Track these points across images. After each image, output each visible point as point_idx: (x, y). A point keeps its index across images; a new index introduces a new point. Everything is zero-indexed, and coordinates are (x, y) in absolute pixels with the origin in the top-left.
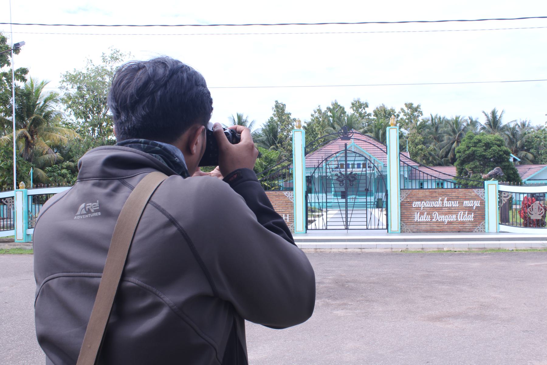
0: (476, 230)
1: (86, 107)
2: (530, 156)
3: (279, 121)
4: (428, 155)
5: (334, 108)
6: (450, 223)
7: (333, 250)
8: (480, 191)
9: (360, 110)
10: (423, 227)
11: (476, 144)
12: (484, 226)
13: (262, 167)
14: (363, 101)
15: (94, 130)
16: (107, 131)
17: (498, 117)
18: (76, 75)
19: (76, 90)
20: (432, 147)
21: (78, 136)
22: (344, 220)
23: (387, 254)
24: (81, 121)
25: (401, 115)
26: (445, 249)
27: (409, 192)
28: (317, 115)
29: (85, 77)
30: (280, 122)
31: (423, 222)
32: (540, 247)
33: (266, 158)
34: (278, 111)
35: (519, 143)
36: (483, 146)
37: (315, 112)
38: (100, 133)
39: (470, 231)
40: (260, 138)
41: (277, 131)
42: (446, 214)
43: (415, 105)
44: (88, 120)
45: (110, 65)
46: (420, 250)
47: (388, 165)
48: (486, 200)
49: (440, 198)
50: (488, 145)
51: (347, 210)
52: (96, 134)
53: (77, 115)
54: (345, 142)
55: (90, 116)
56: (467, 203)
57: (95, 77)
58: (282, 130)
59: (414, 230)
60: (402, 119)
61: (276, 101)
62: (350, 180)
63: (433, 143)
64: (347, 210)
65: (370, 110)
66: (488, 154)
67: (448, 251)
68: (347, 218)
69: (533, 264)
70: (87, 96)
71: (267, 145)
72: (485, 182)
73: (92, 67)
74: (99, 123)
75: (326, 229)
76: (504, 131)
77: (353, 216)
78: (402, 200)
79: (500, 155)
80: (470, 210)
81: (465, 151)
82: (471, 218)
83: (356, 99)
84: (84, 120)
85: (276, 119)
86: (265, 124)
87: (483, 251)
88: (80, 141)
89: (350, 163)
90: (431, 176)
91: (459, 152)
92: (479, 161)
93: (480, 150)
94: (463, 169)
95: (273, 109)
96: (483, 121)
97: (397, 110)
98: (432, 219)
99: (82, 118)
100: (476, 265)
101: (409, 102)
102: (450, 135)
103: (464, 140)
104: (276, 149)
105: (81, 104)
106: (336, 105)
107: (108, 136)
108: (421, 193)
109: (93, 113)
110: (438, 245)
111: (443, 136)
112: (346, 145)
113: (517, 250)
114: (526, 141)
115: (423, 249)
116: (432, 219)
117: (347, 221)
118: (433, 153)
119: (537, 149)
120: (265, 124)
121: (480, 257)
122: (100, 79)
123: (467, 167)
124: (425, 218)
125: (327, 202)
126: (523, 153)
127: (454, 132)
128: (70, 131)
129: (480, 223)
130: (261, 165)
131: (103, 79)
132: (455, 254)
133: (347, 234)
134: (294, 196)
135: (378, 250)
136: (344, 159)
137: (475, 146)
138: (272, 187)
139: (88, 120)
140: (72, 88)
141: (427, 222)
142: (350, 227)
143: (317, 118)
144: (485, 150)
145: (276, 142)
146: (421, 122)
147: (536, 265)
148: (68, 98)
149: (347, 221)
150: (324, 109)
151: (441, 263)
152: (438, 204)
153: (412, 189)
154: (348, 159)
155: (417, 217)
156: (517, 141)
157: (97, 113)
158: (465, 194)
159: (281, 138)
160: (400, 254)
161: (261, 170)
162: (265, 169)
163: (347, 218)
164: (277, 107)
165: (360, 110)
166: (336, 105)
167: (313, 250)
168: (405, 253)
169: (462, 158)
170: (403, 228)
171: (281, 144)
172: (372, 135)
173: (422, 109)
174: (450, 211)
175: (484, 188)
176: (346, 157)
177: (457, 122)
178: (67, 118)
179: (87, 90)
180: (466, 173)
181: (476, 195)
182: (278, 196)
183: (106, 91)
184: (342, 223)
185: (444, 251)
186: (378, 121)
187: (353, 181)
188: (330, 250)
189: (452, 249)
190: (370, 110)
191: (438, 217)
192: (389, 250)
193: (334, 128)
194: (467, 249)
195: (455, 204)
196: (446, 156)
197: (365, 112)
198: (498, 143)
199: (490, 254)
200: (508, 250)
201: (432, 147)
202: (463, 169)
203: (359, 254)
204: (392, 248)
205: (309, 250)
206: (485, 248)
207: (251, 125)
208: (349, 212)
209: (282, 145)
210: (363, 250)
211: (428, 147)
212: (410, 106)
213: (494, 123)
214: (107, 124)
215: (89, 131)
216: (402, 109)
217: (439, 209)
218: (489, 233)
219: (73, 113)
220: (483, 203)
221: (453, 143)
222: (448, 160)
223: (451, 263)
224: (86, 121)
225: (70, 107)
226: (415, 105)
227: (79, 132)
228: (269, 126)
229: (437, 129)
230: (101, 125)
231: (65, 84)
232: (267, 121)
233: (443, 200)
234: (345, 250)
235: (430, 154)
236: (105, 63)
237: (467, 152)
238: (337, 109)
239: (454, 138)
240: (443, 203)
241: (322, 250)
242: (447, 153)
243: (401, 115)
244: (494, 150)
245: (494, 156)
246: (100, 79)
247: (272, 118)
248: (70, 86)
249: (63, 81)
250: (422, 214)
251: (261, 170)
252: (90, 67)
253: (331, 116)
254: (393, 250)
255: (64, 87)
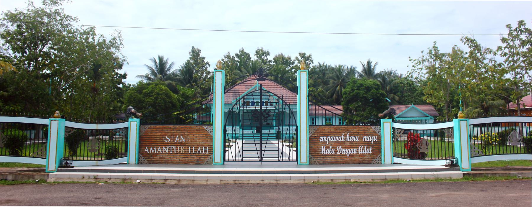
0: (373, 162)
1: (24, 43)
2: (397, 98)
3: (194, 64)
4: (317, 96)
5: (241, 55)
6: (352, 155)
7: (251, 182)
8: (377, 128)
9: (263, 57)
10: (329, 159)
11: (358, 88)
12: (381, 158)
13: (179, 102)
14: (265, 49)
15: (29, 64)
16: (42, 66)
17: (372, 67)
18: (17, 14)
19: (16, 28)
20: (320, 89)
21: (13, 68)
22: (259, 152)
23: (302, 186)
24: (18, 55)
25: (296, 63)
26: (352, 180)
27: (316, 128)
28: (226, 60)
29: (25, 17)
30: (196, 64)
31: (328, 155)
32: (431, 178)
33: (183, 94)
34: (194, 55)
35: (388, 88)
36: (365, 89)
37: (225, 58)
38: (35, 67)
39: (369, 163)
40: (178, 77)
41: (192, 72)
42: (348, 148)
43: (307, 55)
44: (25, 55)
45: (50, 7)
46: (330, 181)
47: (298, 104)
48: (382, 135)
49: (344, 134)
50: (368, 89)
51: (261, 144)
52: (31, 68)
53: (14, 50)
54: (261, 82)
55: (27, 51)
56: (366, 138)
57: (34, 17)
58: (197, 71)
59: (321, 162)
60: (296, 66)
61: (193, 47)
62: (264, 117)
63: (321, 86)
64: (261, 144)
65: (270, 58)
66: (368, 96)
67: (354, 182)
68: (261, 150)
69: (433, 195)
70: (26, 34)
71: (184, 84)
72: (381, 120)
73: (33, 8)
74: (34, 59)
75: (242, 161)
76: (377, 78)
77: (267, 149)
78: (311, 135)
79: (378, 97)
80: (368, 144)
81: (350, 93)
82: (369, 151)
83: (260, 48)
84: (20, 54)
85: (192, 62)
86: (183, 65)
87: (385, 182)
88: (15, 73)
89: (264, 101)
90: (332, 113)
91: (345, 93)
92: (361, 101)
93: (362, 92)
94: (348, 108)
95: (190, 53)
96: (360, 69)
97: (293, 58)
98: (336, 152)
99: (19, 53)
100: (385, 196)
101: (303, 52)
102: (334, 80)
103: (349, 85)
104: (192, 87)
105: (19, 40)
106: (242, 52)
107: (43, 71)
108: (327, 129)
109: (30, 49)
110: (345, 176)
111: (329, 81)
112: (261, 85)
113: (413, 181)
114: (394, 86)
115: (332, 180)
116: (336, 152)
117: (261, 154)
118: (321, 94)
119: (402, 92)
120: (183, 65)
121: (384, 188)
122: (39, 19)
123: (351, 106)
124: (330, 151)
125: (243, 134)
126: (392, 95)
127: (337, 77)
128: (5, 64)
129: (377, 155)
130: (179, 100)
131: (42, 19)
132: (362, 185)
133: (261, 166)
134: (214, 131)
135: (292, 182)
136: (259, 97)
137: (358, 89)
138: (187, 120)
139: (25, 55)
140: (12, 25)
141: (332, 155)
142: (264, 159)
143: (227, 62)
144: (366, 93)
145: (192, 81)
146: (312, 69)
147: (437, 196)
148: (7, 34)
149: (261, 154)
150: (232, 54)
151: (353, 195)
152: (341, 139)
153: (319, 125)
154: (263, 97)
155: (323, 151)
156: (387, 86)
157: (34, 49)
158: (364, 130)
159: (196, 78)
160: (314, 186)
161: (178, 105)
162: (182, 104)
163: (261, 150)
164: (193, 51)
165: (263, 57)
166: (242, 52)
167: (232, 182)
168: (316, 185)
169: (348, 99)
170: (311, 160)
171: (196, 83)
172: (272, 78)
173: (313, 58)
174: (352, 145)
175: (380, 125)
176: (261, 96)
177: (339, 70)
178: (5, 52)
179: (26, 28)
180: (351, 110)
181: (374, 132)
182: (199, 130)
183: (44, 30)
184: (257, 156)
185: (351, 183)
186: (278, 67)
187: (267, 117)
188: (248, 182)
189: (358, 181)
190: (270, 58)
191: (341, 151)
192: (302, 182)
193: (241, 71)
194: (371, 181)
195: (356, 139)
196: (332, 97)
197: (267, 59)
198: (376, 87)
199: (392, 185)
200: (406, 181)
201: (320, 89)
202: (348, 108)
203: (276, 186)
204: (304, 180)
205: (228, 182)
206: (386, 179)
207: (170, 66)
208: (263, 145)
209: (196, 84)
210: (279, 182)
211: (317, 89)
212: (303, 55)
213: (368, 70)
214: (43, 59)
215: (25, 64)
216: (297, 58)
217: (342, 144)
218: (385, 165)
219: (10, 48)
220: (379, 138)
221: (337, 86)
222: (333, 100)
223: (362, 195)
224: (23, 56)
225: (8, 42)
226: (307, 55)
227: (16, 65)
228: (185, 67)
229: (324, 74)
230: (37, 59)
231: (5, 22)
232: (185, 63)
233: (345, 136)
234: (262, 182)
235: (319, 95)
236: (44, 6)
237: (352, 94)
238: (243, 55)
239: (338, 82)
240: (346, 138)
241: (241, 182)
242: (332, 94)
243: (296, 63)
244: (373, 93)
245: (373, 98)
246: (39, 19)
247: (188, 61)
248: (9, 24)
249: (4, 19)
250: (327, 147)
251: (178, 105)
252: (31, 8)
253: (238, 61)
254: (306, 182)
255: (5, 25)
